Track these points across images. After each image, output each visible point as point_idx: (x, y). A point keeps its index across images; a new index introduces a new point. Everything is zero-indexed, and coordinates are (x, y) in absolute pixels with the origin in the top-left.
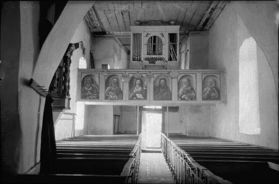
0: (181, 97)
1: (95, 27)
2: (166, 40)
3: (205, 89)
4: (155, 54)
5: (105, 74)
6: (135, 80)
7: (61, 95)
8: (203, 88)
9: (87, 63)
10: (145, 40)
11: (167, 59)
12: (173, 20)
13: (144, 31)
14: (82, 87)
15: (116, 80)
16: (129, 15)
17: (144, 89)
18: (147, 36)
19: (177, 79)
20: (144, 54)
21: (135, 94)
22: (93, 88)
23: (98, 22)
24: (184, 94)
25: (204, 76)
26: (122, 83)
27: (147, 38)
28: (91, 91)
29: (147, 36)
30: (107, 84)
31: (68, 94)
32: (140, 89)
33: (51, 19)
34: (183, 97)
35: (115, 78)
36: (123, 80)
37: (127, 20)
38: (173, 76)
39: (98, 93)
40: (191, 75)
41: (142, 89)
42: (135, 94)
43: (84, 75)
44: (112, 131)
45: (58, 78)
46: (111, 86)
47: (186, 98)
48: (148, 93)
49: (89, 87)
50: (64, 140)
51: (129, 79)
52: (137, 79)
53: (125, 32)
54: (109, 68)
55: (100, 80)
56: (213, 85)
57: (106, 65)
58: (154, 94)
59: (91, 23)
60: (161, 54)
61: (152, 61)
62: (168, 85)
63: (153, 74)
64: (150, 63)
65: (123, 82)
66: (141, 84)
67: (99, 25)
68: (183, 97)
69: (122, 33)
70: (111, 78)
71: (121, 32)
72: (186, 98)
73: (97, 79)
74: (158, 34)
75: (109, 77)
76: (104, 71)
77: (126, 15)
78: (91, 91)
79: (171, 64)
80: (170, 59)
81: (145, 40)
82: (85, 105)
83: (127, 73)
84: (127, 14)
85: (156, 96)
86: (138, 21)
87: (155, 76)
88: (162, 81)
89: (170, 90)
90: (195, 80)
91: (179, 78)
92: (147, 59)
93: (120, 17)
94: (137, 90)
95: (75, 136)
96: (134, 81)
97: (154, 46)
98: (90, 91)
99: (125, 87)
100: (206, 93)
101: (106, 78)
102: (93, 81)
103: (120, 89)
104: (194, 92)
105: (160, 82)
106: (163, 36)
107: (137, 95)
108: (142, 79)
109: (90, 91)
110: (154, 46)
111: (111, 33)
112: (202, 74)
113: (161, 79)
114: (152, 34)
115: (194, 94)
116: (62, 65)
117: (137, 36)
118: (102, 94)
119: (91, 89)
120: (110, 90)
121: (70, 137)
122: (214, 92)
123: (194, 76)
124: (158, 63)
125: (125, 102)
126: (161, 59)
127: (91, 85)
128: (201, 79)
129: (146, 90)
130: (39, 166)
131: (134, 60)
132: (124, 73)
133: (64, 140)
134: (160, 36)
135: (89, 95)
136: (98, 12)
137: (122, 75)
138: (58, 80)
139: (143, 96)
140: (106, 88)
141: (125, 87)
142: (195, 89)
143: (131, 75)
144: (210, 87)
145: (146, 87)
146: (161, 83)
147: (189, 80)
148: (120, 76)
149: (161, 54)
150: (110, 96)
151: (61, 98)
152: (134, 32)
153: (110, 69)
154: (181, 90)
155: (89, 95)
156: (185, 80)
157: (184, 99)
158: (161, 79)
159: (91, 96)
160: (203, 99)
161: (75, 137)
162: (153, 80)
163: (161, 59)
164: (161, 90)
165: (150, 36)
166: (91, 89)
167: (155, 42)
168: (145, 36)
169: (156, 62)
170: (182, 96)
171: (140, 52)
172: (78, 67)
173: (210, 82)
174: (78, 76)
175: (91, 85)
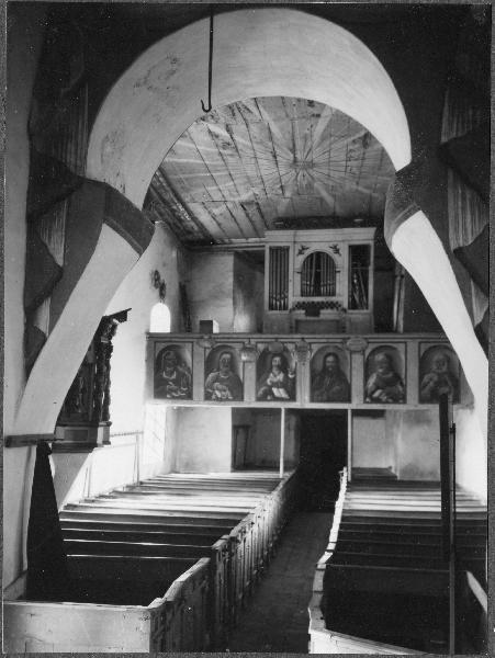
0: (371, 396)
1: (189, 232)
2: (343, 261)
3: (426, 379)
4: (319, 294)
5: (207, 345)
6: (270, 356)
7: (90, 419)
8: (421, 378)
9: (173, 312)
10: (296, 262)
11: (346, 305)
12: (360, 216)
13: (295, 242)
14: (155, 374)
15: (228, 356)
16: (259, 209)
17: (290, 376)
18: (300, 253)
19: (364, 354)
20: (294, 295)
21: (270, 387)
22: (181, 376)
23: (193, 224)
24: (378, 388)
25: (424, 347)
26: (241, 364)
27: (301, 258)
28: (176, 382)
29: (300, 253)
30: (209, 365)
31: (106, 416)
32: (281, 377)
33: (43, 325)
34: (376, 394)
35: (226, 353)
36: (244, 358)
37: (257, 218)
38: (353, 348)
39: (189, 385)
40: (395, 345)
41: (286, 376)
42: (270, 387)
43: (161, 346)
44: (228, 462)
45: (84, 388)
46: (218, 370)
47: (384, 398)
48: (298, 383)
49: (172, 373)
50: (116, 494)
51: (258, 354)
52: (275, 355)
53: (257, 239)
54: (216, 329)
55: (194, 357)
56: (444, 369)
57: (210, 323)
58: (313, 390)
59: (179, 225)
60: (334, 294)
61: (313, 309)
62: (342, 368)
63: (310, 344)
64: (307, 314)
65: (244, 362)
66: (284, 367)
67: (196, 228)
68: (376, 394)
69: (250, 240)
70: (220, 359)
71: (247, 238)
72: (384, 398)
73: (188, 356)
74: (326, 248)
75: (214, 351)
76: (202, 338)
77: (252, 210)
78: (176, 382)
79: (353, 316)
80: (353, 305)
81: (296, 262)
82: (350, 246)
83: (253, 342)
84: (255, 207)
85: (317, 393)
86: (280, 219)
87: (315, 348)
88: (330, 359)
89: (346, 380)
90: (403, 357)
91: (368, 352)
92: (299, 306)
93: (239, 214)
94: (275, 380)
95: (141, 479)
96: (269, 360)
97: (318, 275)
98: (173, 381)
99: (248, 374)
100: (428, 388)
101: (208, 351)
102: (179, 360)
103: (238, 376)
104: (401, 383)
105: (325, 361)
106: (337, 251)
107: (275, 390)
108: (285, 354)
109: (173, 381)
110: (318, 275)
111: (227, 241)
112: (420, 343)
113: (329, 354)
114: (314, 248)
115: (401, 389)
116: (91, 361)
117: (280, 254)
118: (199, 390)
119: (174, 377)
120: (217, 379)
121: (130, 482)
122: (446, 383)
123: (401, 347)
124: (326, 314)
125: (250, 401)
126: (332, 305)
127: (176, 369)
128: (417, 353)
129: (294, 381)
130: (22, 581)
131: (272, 307)
132: (246, 342)
133: (116, 494)
134: (330, 252)
135: (172, 390)
136: (191, 206)
137: (241, 346)
138: (84, 390)
139: (288, 392)
140: (206, 375)
141: (248, 374)
142: (403, 377)
143: (261, 347)
144: (439, 374)
145: (295, 373)
146: (328, 364)
147: (388, 356)
148: (238, 347)
149: (333, 294)
150: (217, 392)
151: (91, 426)
152: (272, 245)
153: (220, 334)
154: (372, 381)
155: (172, 390)
156: (380, 357)
157: (377, 400)
158: (329, 354)
159: (176, 391)
160: (422, 400)
161: (141, 483)
162: (309, 356)
163: (332, 305)
164: (327, 381)
165: (307, 253)
166: (174, 377)
167: (318, 266)
168: (297, 252)
169: (322, 311)
170: (373, 392)
171: (286, 289)
172: (149, 326)
173: (437, 362)
174: (148, 347)
175: (176, 369)
